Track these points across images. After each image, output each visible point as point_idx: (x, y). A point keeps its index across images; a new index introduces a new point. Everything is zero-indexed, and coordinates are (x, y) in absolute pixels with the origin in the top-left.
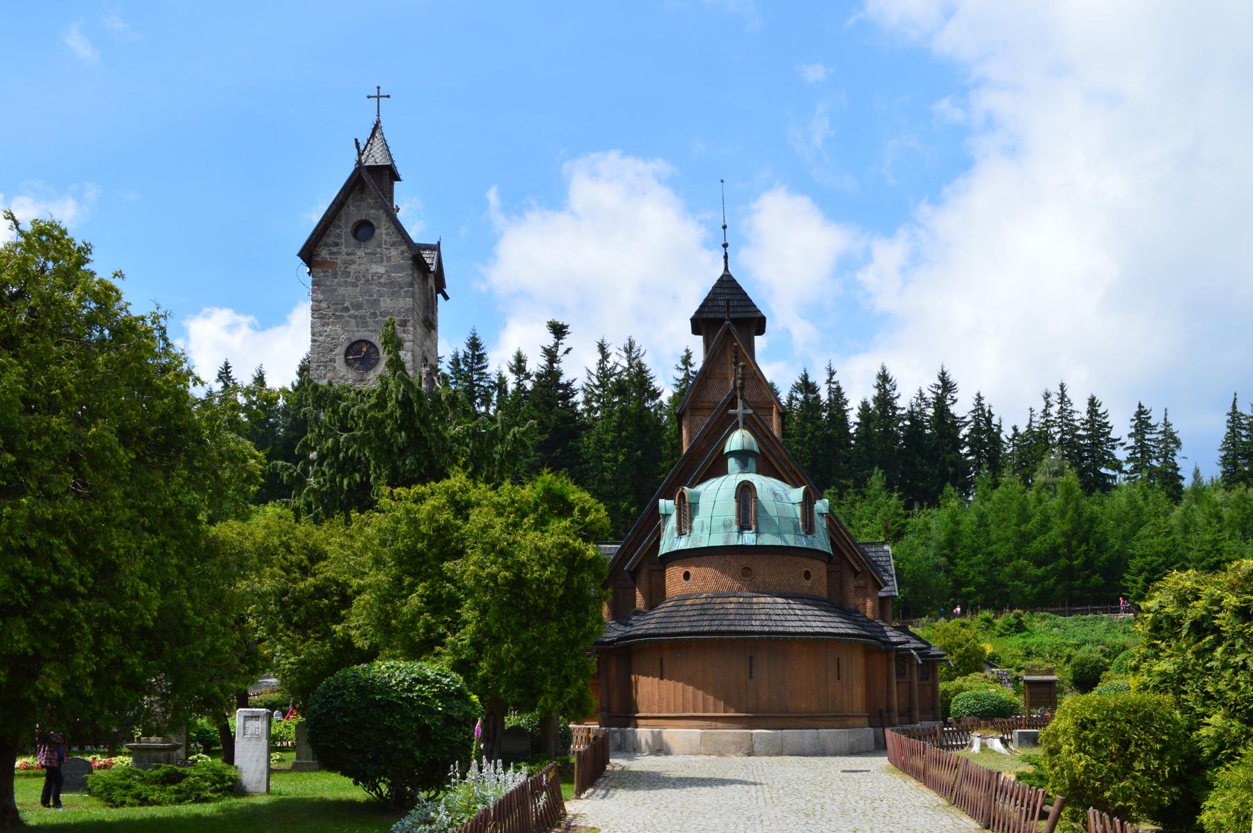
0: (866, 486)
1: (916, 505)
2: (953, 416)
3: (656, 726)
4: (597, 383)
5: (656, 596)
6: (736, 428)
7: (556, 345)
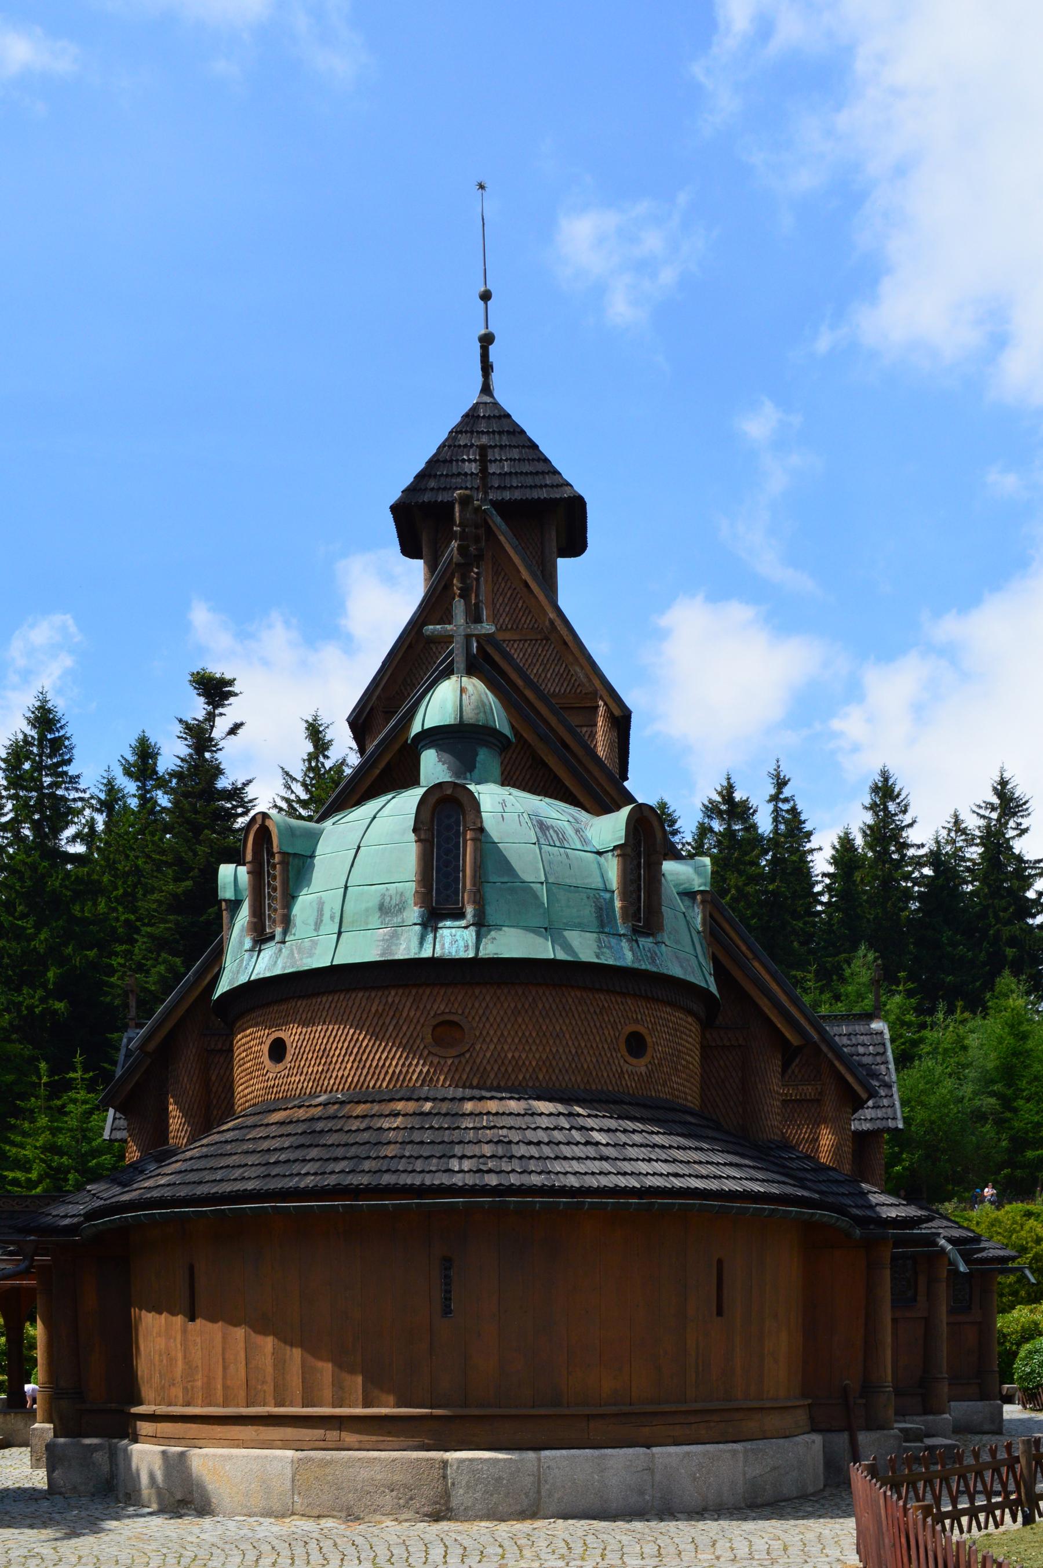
0: (843, 980)
1: (942, 1006)
2: (1019, 859)
3: (177, 1440)
4: (304, 796)
5: (213, 1106)
6: (447, 673)
7: (211, 717)
